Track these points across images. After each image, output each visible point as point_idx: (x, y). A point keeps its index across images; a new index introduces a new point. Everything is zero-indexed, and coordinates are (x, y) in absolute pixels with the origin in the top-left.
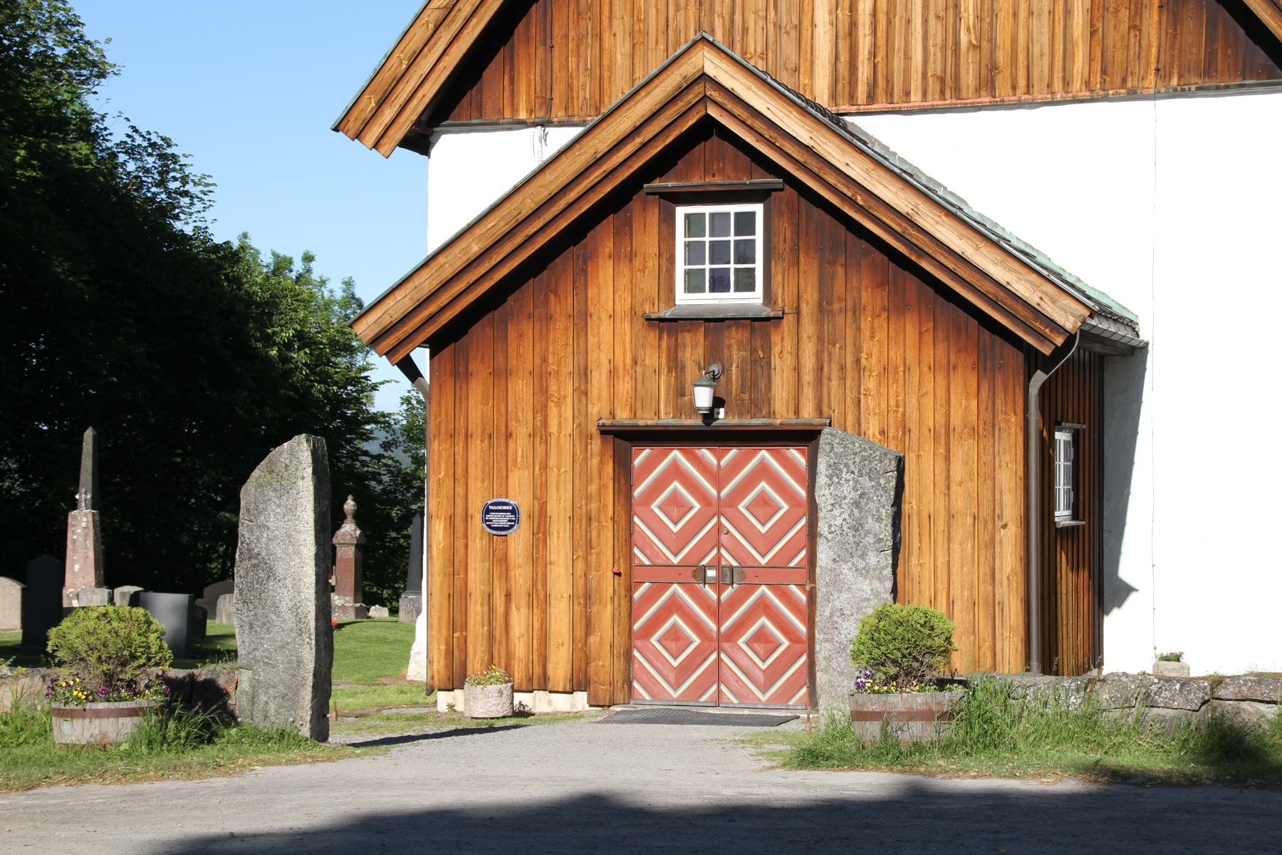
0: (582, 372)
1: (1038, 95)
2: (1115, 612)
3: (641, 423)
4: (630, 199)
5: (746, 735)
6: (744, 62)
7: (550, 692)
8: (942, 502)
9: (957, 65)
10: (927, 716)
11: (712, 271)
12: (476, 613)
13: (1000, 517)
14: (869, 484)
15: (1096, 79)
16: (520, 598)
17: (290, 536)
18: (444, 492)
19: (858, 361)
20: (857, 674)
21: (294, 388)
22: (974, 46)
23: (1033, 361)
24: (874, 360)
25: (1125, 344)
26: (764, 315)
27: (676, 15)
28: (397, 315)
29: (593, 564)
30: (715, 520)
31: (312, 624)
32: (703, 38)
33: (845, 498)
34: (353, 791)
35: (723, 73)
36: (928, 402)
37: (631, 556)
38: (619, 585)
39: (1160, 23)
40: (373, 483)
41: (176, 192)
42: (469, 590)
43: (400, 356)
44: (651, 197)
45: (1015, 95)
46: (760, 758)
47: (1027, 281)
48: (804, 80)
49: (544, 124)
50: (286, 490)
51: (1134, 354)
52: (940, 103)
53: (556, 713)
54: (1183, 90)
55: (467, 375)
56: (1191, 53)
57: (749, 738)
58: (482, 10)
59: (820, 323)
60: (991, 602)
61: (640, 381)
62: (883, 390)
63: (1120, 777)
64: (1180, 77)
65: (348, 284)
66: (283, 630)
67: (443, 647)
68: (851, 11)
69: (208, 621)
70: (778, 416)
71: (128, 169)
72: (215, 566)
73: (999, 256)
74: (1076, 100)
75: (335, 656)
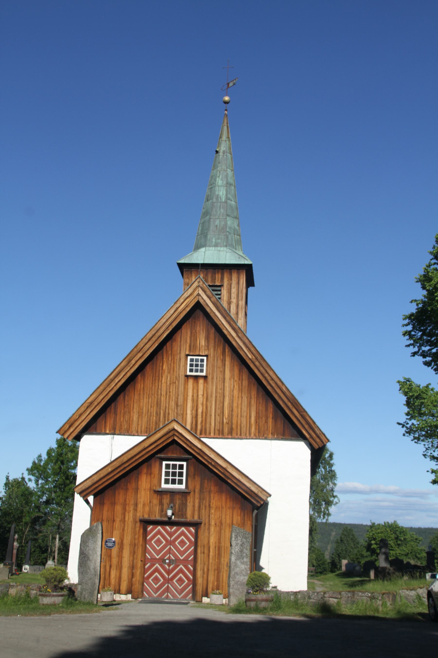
3: (152, 519)
14: (245, 540)
15: (257, 434)
16: (114, 567)
19: (210, 505)
24: (214, 505)
30: (169, 546)
32: (175, 420)
36: (228, 517)
37: (146, 556)
39: (272, 422)
43: (85, 498)
61: (151, 507)
64: (277, 435)
66: (91, 574)
74: (252, 439)
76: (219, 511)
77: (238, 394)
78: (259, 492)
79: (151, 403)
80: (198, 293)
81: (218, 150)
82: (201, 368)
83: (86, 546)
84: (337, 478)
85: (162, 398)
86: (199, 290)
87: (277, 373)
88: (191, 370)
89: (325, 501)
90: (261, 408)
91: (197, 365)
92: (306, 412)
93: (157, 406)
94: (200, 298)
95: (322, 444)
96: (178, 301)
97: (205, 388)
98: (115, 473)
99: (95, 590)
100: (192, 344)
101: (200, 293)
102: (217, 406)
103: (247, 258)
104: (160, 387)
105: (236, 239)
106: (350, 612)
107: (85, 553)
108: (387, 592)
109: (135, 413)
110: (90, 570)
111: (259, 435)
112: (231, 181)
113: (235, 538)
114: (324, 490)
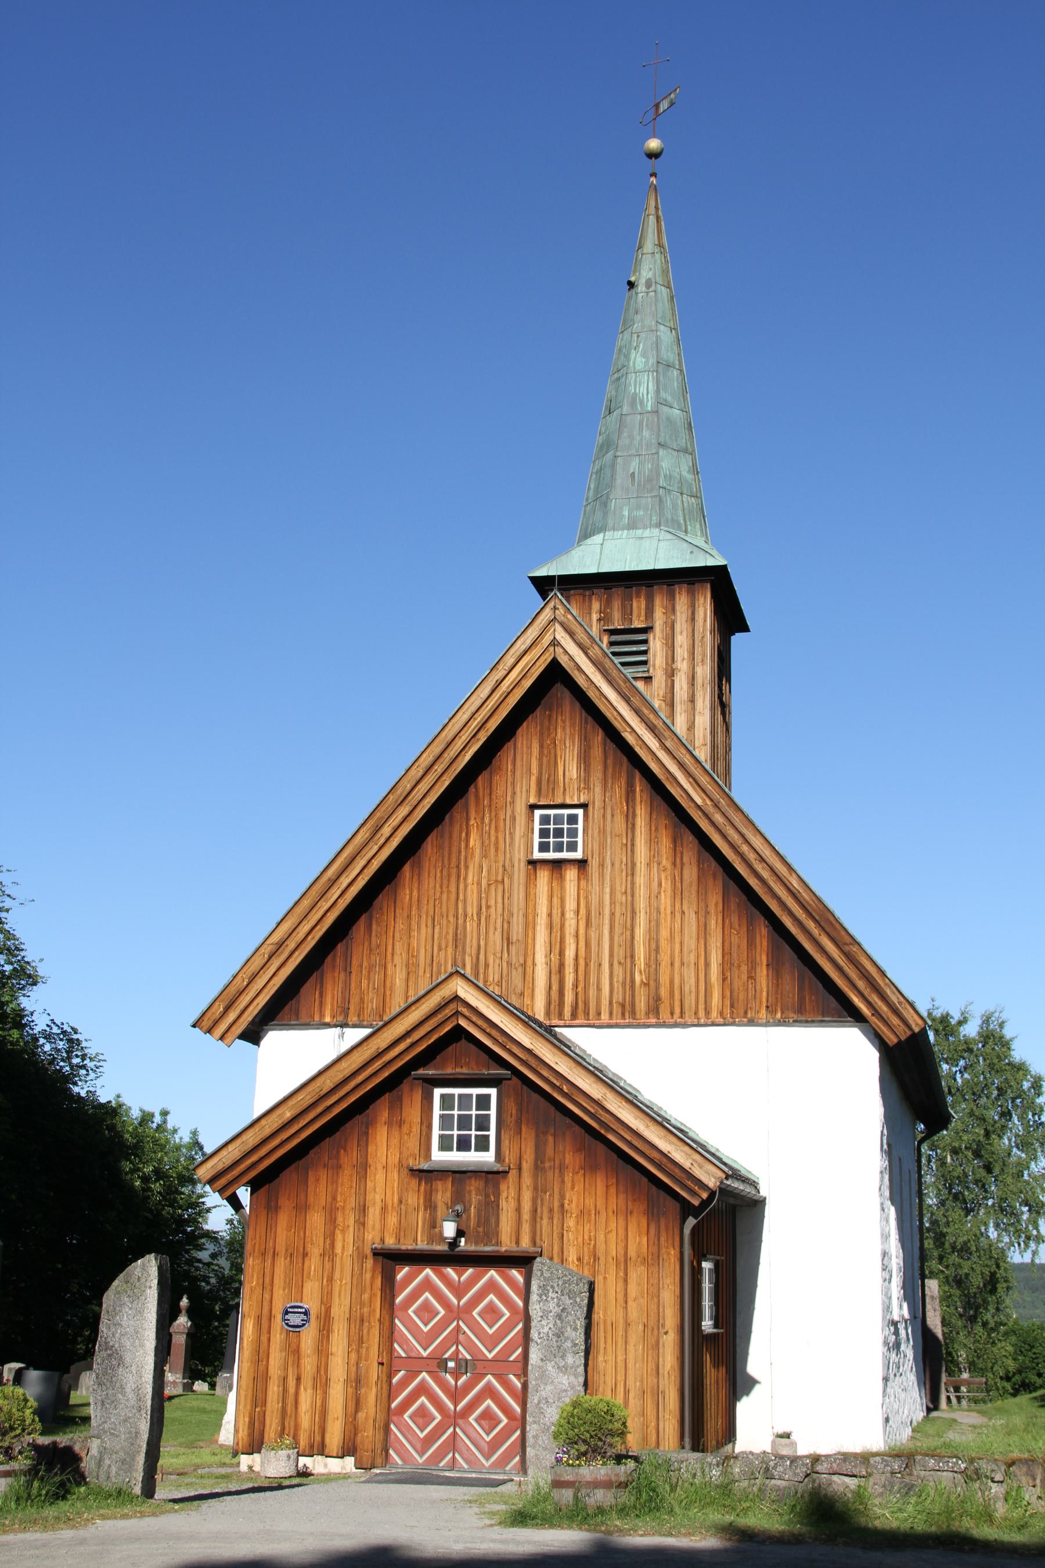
0: (362, 1208)
1: (689, 1019)
2: (745, 1399)
3: (403, 1247)
4: (401, 1082)
6: (486, 989)
7: (327, 1457)
9: (633, 996)
10: (607, 1485)
11: (459, 1136)
12: (273, 1392)
13: (663, 1326)
14: (568, 1302)
15: (727, 1011)
17: (137, 1332)
18: (255, 1297)
19: (562, 1206)
20: (557, 1450)
21: (150, 1211)
22: (645, 984)
23: (687, 1209)
24: (574, 1205)
25: (750, 1198)
26: (495, 1169)
27: (438, 953)
29: (363, 1356)
30: (455, 1323)
31: (149, 1403)
32: (457, 972)
33: (551, 1312)
34: (171, 1543)
36: (612, 1237)
37: (392, 1350)
39: (768, 975)
40: (203, 1284)
41: (77, 1066)
43: (229, 1193)
44: (416, 1082)
45: (672, 1018)
46: (483, 1516)
47: (682, 1151)
48: (527, 1001)
50: (137, 1296)
51: (755, 1206)
53: (329, 1474)
55: (277, 1209)
56: (789, 997)
57: (475, 1498)
59: (535, 1177)
60: (656, 1391)
62: (580, 1228)
63: (746, 1536)
64: (782, 1013)
65: (195, 1133)
66: (127, 1407)
67: (247, 1419)
68: (560, 956)
69: (72, 1392)
71: (45, 1050)
72: (81, 1347)
73: (663, 1132)
74: (713, 1024)
76: (589, 1221)
77: (673, 906)
78: (695, 1165)
79: (440, 938)
81: (633, 279)
83: (115, 1325)
88: (544, 847)
89: (1026, 1203)
90: (735, 940)
91: (559, 833)
93: (456, 947)
94: (559, 650)
96: (501, 662)
97: (582, 892)
98: (302, 1122)
100: (545, 777)
101: (558, 637)
103: (714, 552)
104: (461, 897)
108: (1026, 1455)
109: (398, 968)
112: (670, 355)
113: (540, 1296)
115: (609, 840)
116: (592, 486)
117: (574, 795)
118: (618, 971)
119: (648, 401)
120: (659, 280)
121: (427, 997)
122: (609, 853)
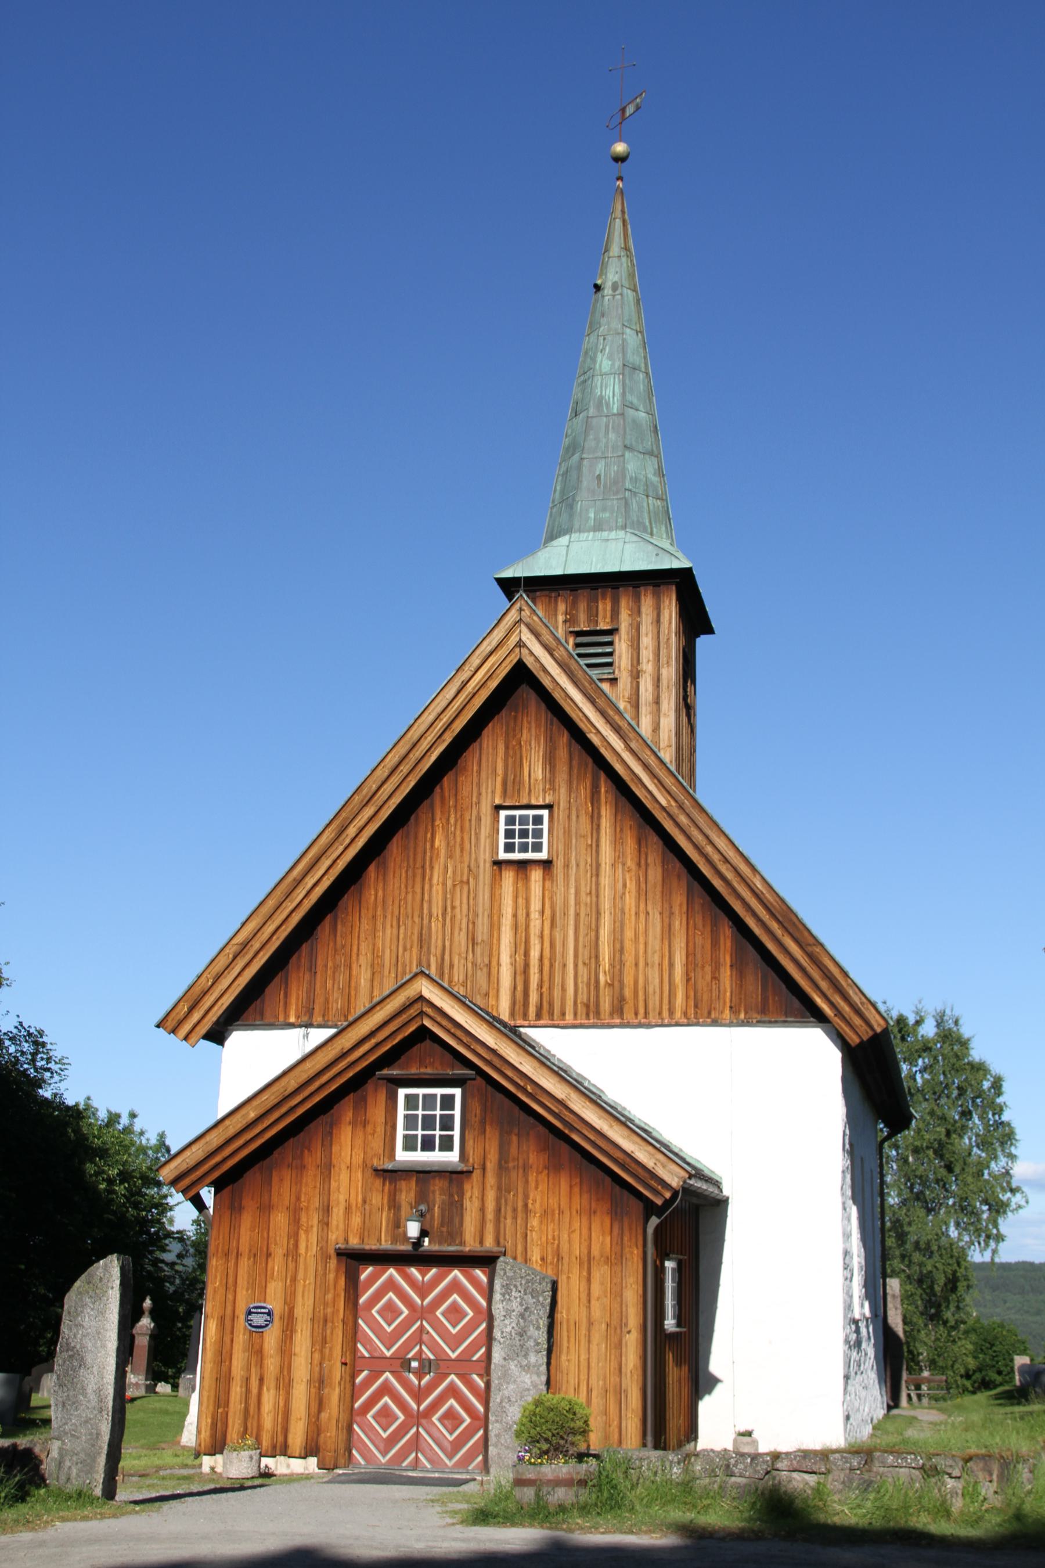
0: (326, 1208)
3: (367, 1247)
5: (435, 1495)
6: (450, 989)
7: (289, 1457)
8: (585, 1313)
9: (597, 997)
10: (568, 1483)
11: (423, 1136)
13: (626, 1325)
14: (531, 1301)
15: (691, 1011)
19: (526, 1205)
20: (519, 1449)
21: (114, 1213)
23: (650, 1209)
24: (538, 1205)
26: (459, 1169)
28: (192, 1162)
30: (419, 1323)
31: (110, 1404)
32: (422, 972)
33: (514, 1311)
35: (435, 996)
36: (576, 1236)
37: (355, 1349)
38: (345, 1372)
39: (731, 976)
42: (232, 1375)
43: (192, 1193)
44: (381, 1082)
47: (645, 1151)
48: (492, 1002)
49: (307, 1026)
50: (99, 1296)
51: (720, 1205)
52: (586, 1021)
53: (292, 1475)
54: (748, 1022)
55: (241, 1209)
57: (437, 1498)
58: (268, 946)
59: (499, 1177)
60: (618, 1389)
64: (746, 1013)
66: (88, 1408)
67: (209, 1421)
68: (525, 956)
70: (467, 1244)
73: (626, 1132)
74: (677, 1024)
75: (127, 1424)
76: (553, 1221)
77: (638, 906)
79: (405, 938)
80: (518, 639)
81: (599, 282)
82: (534, 840)
83: (76, 1326)
84: (1016, 1140)
85: (433, 924)
86: (520, 632)
87: (736, 843)
88: (509, 848)
89: (985, 1202)
90: (699, 940)
91: (524, 834)
92: (822, 945)
94: (524, 651)
95: (868, 1030)
96: (467, 663)
97: (547, 893)
99: (99, 1454)
100: (511, 778)
101: (524, 638)
102: (581, 939)
103: (679, 555)
105: (651, 507)
106: (855, 1515)
107: (74, 1347)
108: (983, 1451)
109: (363, 968)
110: (86, 1397)
111: (696, 1013)
112: (636, 358)
113: (503, 1295)
114: (983, 1175)
115: (574, 841)
116: (558, 488)
117: (539, 796)
118: (583, 971)
119: (614, 403)
120: (626, 283)
121: (392, 998)
122: (574, 854)
